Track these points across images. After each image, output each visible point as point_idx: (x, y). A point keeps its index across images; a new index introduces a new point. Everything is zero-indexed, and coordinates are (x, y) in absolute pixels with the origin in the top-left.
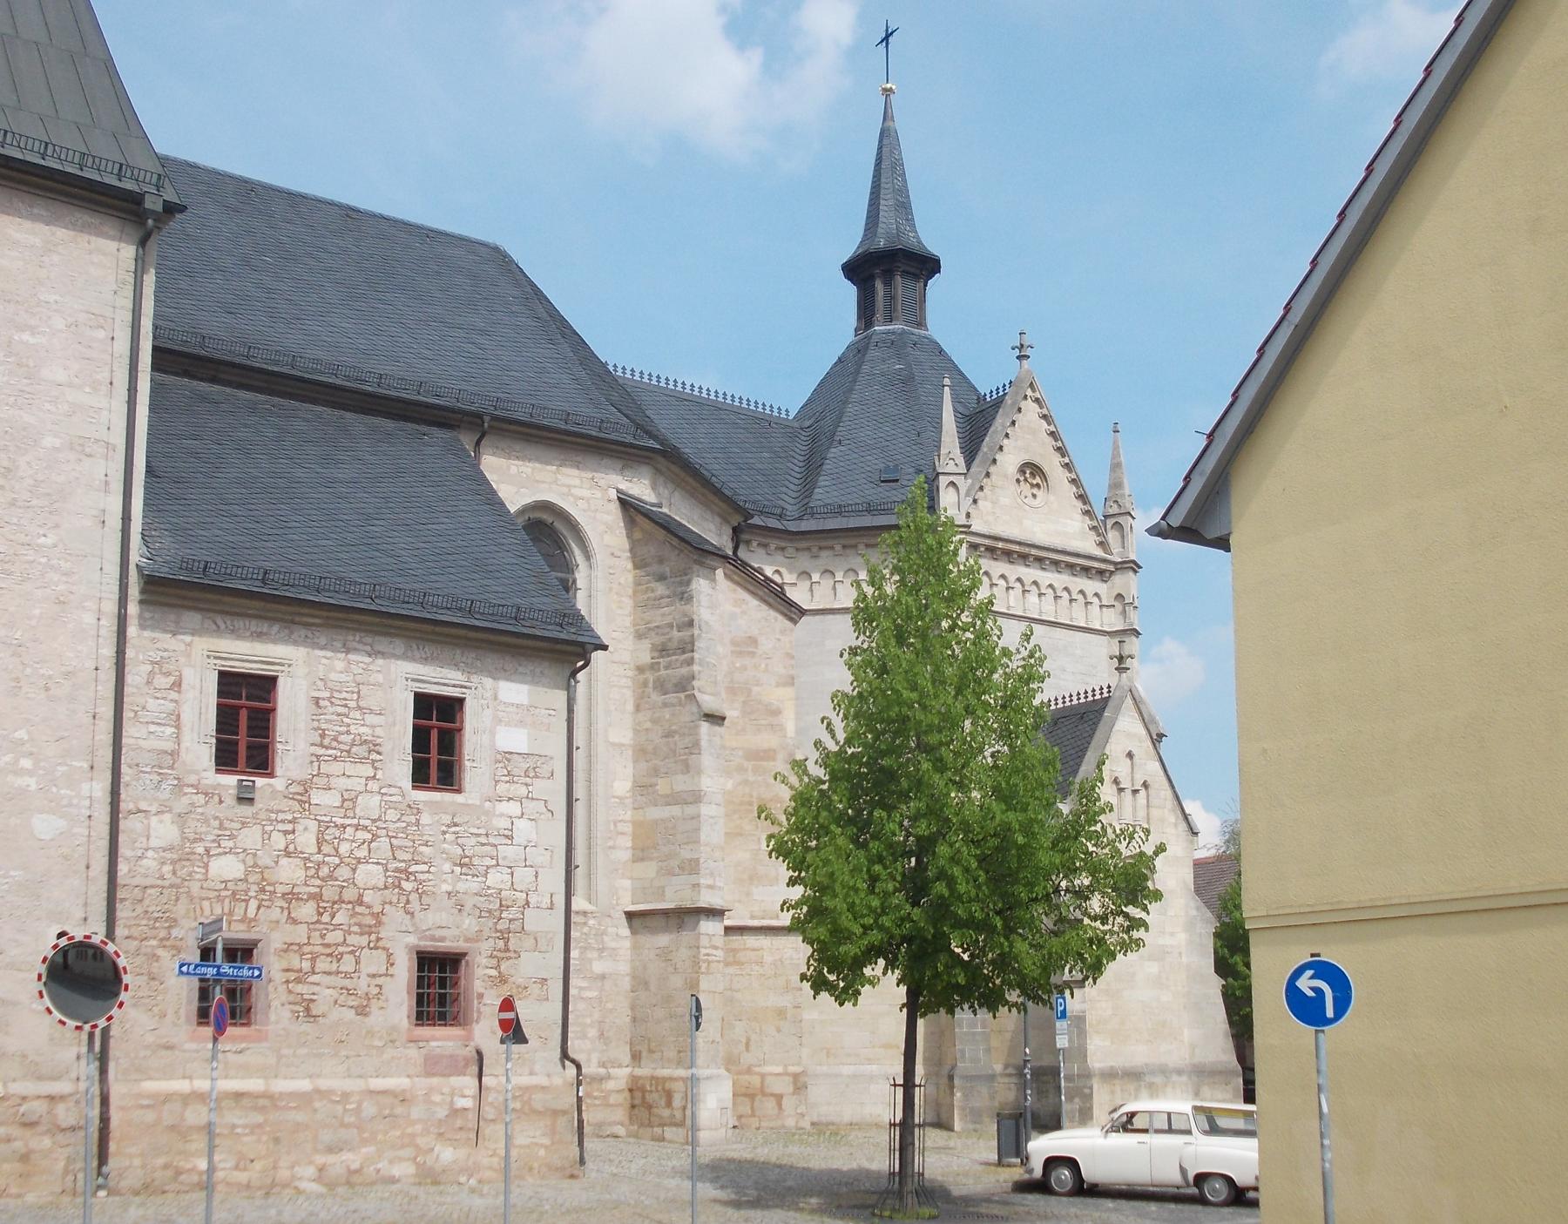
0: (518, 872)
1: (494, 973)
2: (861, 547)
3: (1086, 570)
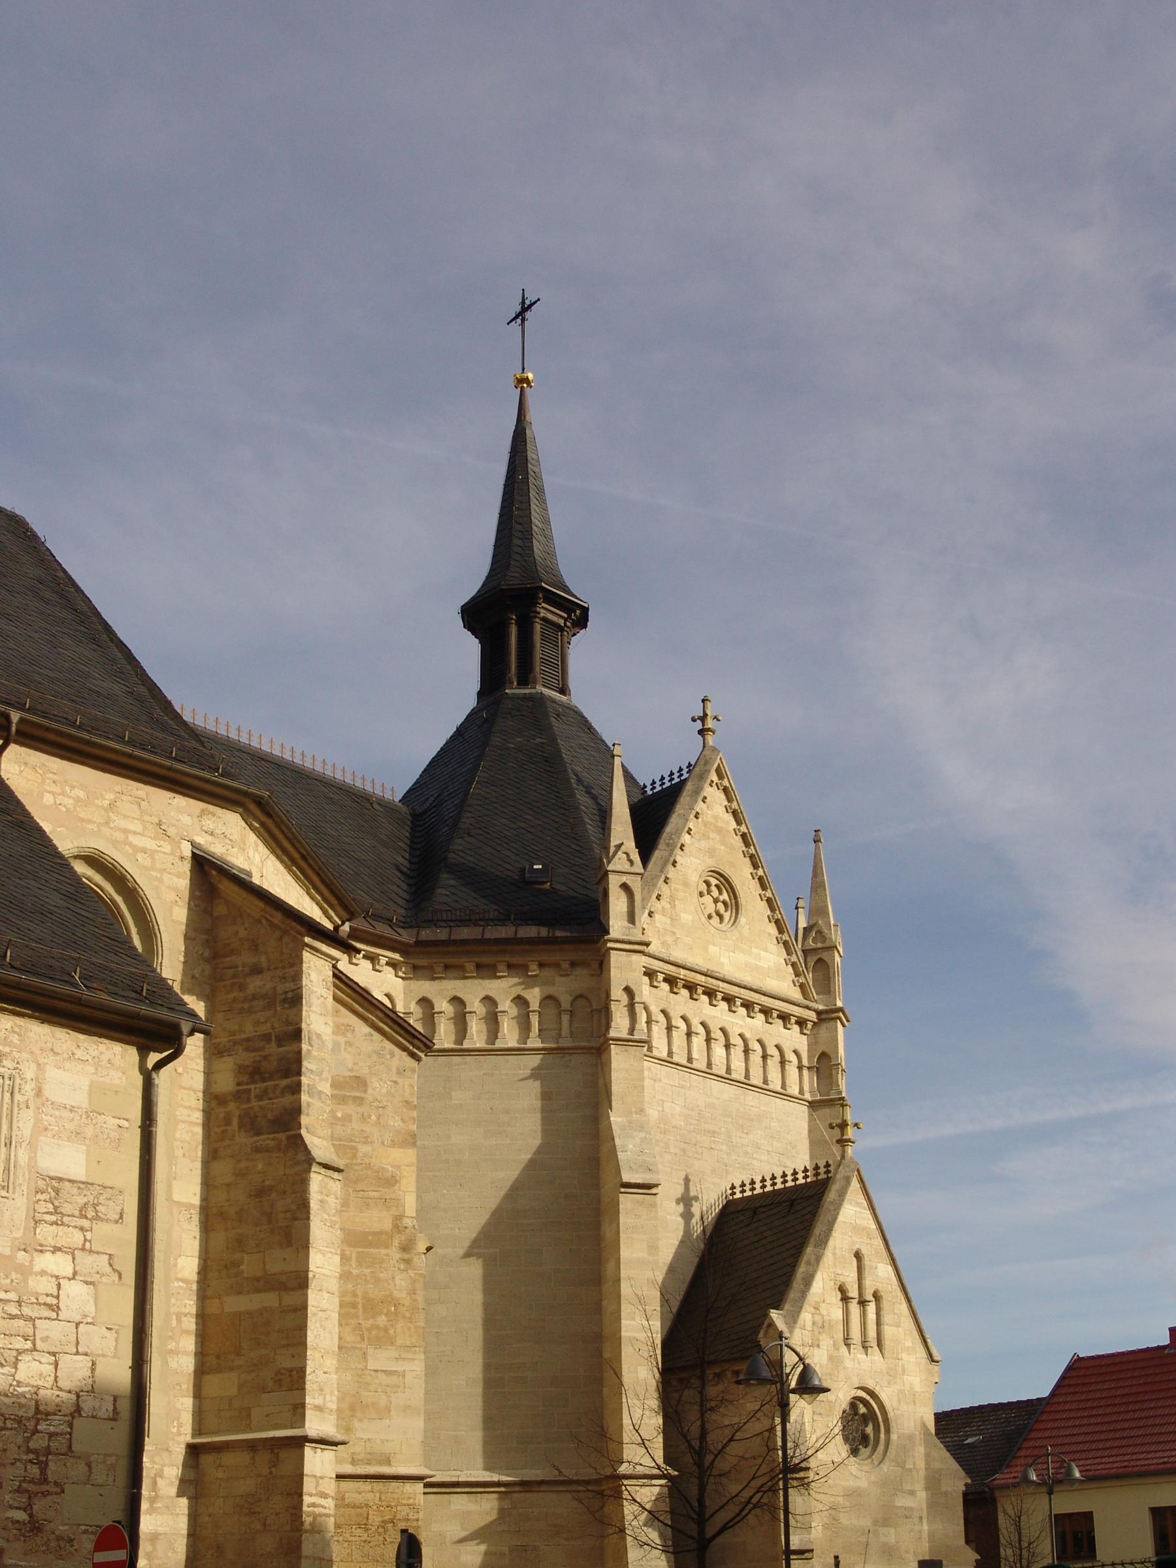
0: (64, 1360)
1: (21, 1516)
2: (501, 967)
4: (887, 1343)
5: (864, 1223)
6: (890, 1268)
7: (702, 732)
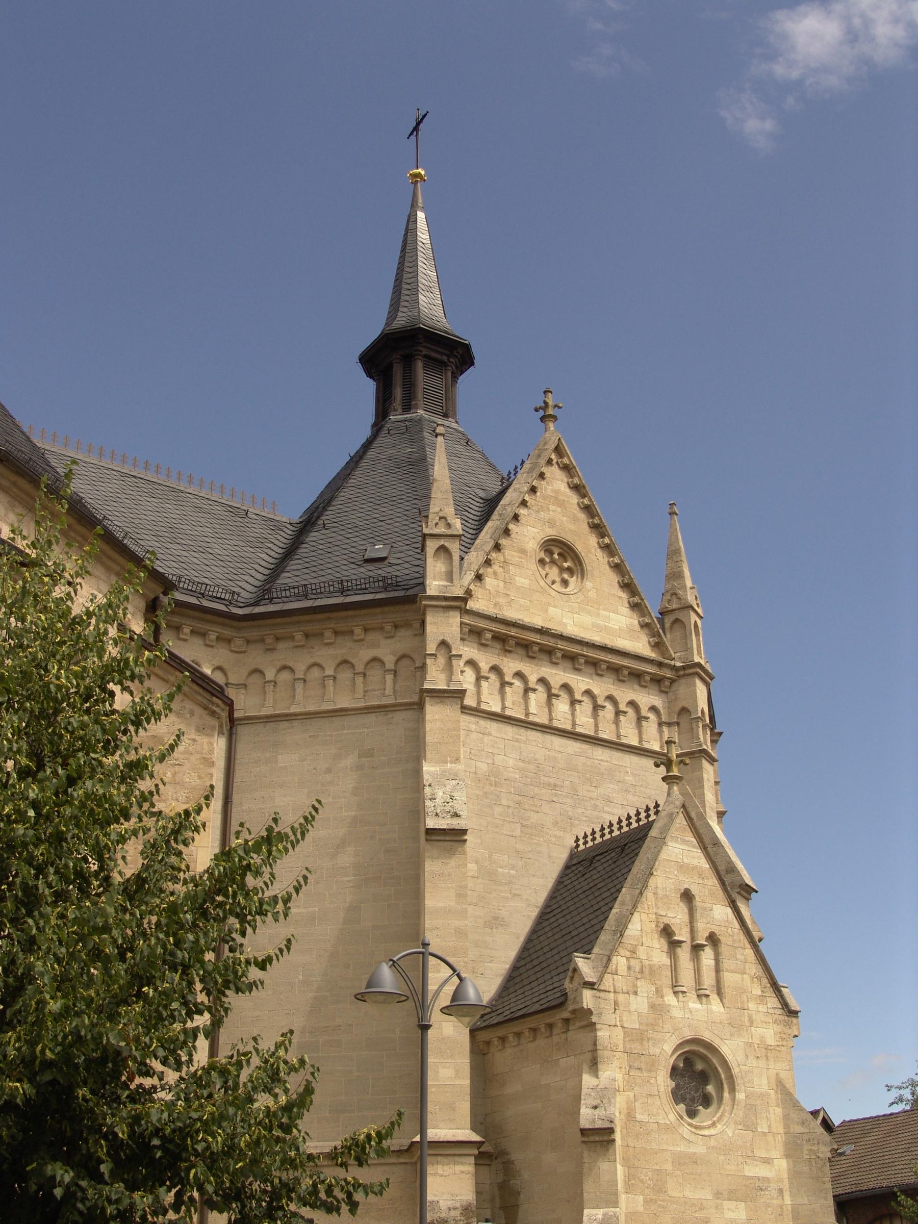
3: (637, 676)
4: (726, 991)
5: (695, 862)
6: (729, 910)
7: (542, 419)
